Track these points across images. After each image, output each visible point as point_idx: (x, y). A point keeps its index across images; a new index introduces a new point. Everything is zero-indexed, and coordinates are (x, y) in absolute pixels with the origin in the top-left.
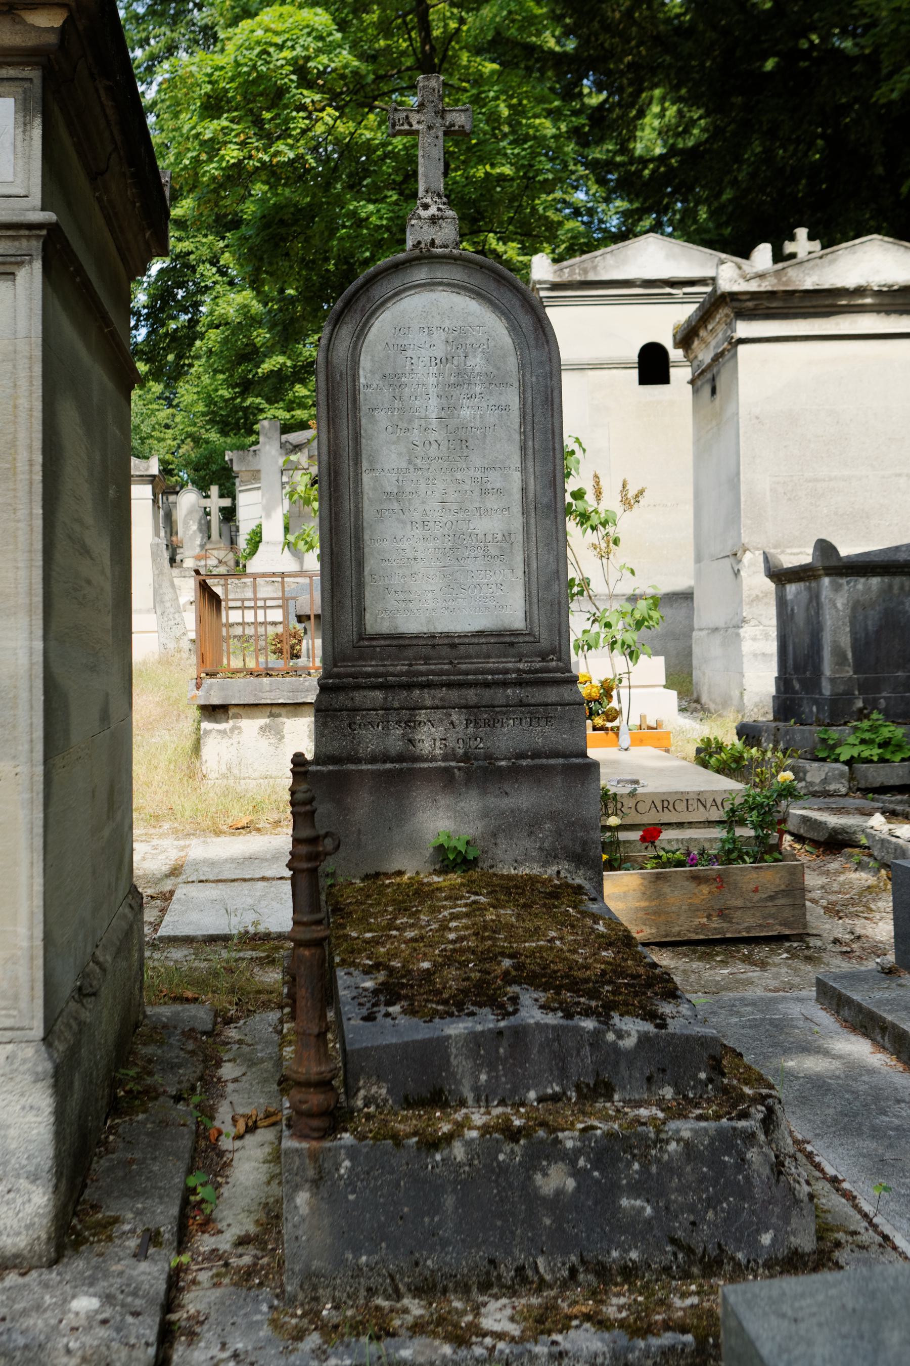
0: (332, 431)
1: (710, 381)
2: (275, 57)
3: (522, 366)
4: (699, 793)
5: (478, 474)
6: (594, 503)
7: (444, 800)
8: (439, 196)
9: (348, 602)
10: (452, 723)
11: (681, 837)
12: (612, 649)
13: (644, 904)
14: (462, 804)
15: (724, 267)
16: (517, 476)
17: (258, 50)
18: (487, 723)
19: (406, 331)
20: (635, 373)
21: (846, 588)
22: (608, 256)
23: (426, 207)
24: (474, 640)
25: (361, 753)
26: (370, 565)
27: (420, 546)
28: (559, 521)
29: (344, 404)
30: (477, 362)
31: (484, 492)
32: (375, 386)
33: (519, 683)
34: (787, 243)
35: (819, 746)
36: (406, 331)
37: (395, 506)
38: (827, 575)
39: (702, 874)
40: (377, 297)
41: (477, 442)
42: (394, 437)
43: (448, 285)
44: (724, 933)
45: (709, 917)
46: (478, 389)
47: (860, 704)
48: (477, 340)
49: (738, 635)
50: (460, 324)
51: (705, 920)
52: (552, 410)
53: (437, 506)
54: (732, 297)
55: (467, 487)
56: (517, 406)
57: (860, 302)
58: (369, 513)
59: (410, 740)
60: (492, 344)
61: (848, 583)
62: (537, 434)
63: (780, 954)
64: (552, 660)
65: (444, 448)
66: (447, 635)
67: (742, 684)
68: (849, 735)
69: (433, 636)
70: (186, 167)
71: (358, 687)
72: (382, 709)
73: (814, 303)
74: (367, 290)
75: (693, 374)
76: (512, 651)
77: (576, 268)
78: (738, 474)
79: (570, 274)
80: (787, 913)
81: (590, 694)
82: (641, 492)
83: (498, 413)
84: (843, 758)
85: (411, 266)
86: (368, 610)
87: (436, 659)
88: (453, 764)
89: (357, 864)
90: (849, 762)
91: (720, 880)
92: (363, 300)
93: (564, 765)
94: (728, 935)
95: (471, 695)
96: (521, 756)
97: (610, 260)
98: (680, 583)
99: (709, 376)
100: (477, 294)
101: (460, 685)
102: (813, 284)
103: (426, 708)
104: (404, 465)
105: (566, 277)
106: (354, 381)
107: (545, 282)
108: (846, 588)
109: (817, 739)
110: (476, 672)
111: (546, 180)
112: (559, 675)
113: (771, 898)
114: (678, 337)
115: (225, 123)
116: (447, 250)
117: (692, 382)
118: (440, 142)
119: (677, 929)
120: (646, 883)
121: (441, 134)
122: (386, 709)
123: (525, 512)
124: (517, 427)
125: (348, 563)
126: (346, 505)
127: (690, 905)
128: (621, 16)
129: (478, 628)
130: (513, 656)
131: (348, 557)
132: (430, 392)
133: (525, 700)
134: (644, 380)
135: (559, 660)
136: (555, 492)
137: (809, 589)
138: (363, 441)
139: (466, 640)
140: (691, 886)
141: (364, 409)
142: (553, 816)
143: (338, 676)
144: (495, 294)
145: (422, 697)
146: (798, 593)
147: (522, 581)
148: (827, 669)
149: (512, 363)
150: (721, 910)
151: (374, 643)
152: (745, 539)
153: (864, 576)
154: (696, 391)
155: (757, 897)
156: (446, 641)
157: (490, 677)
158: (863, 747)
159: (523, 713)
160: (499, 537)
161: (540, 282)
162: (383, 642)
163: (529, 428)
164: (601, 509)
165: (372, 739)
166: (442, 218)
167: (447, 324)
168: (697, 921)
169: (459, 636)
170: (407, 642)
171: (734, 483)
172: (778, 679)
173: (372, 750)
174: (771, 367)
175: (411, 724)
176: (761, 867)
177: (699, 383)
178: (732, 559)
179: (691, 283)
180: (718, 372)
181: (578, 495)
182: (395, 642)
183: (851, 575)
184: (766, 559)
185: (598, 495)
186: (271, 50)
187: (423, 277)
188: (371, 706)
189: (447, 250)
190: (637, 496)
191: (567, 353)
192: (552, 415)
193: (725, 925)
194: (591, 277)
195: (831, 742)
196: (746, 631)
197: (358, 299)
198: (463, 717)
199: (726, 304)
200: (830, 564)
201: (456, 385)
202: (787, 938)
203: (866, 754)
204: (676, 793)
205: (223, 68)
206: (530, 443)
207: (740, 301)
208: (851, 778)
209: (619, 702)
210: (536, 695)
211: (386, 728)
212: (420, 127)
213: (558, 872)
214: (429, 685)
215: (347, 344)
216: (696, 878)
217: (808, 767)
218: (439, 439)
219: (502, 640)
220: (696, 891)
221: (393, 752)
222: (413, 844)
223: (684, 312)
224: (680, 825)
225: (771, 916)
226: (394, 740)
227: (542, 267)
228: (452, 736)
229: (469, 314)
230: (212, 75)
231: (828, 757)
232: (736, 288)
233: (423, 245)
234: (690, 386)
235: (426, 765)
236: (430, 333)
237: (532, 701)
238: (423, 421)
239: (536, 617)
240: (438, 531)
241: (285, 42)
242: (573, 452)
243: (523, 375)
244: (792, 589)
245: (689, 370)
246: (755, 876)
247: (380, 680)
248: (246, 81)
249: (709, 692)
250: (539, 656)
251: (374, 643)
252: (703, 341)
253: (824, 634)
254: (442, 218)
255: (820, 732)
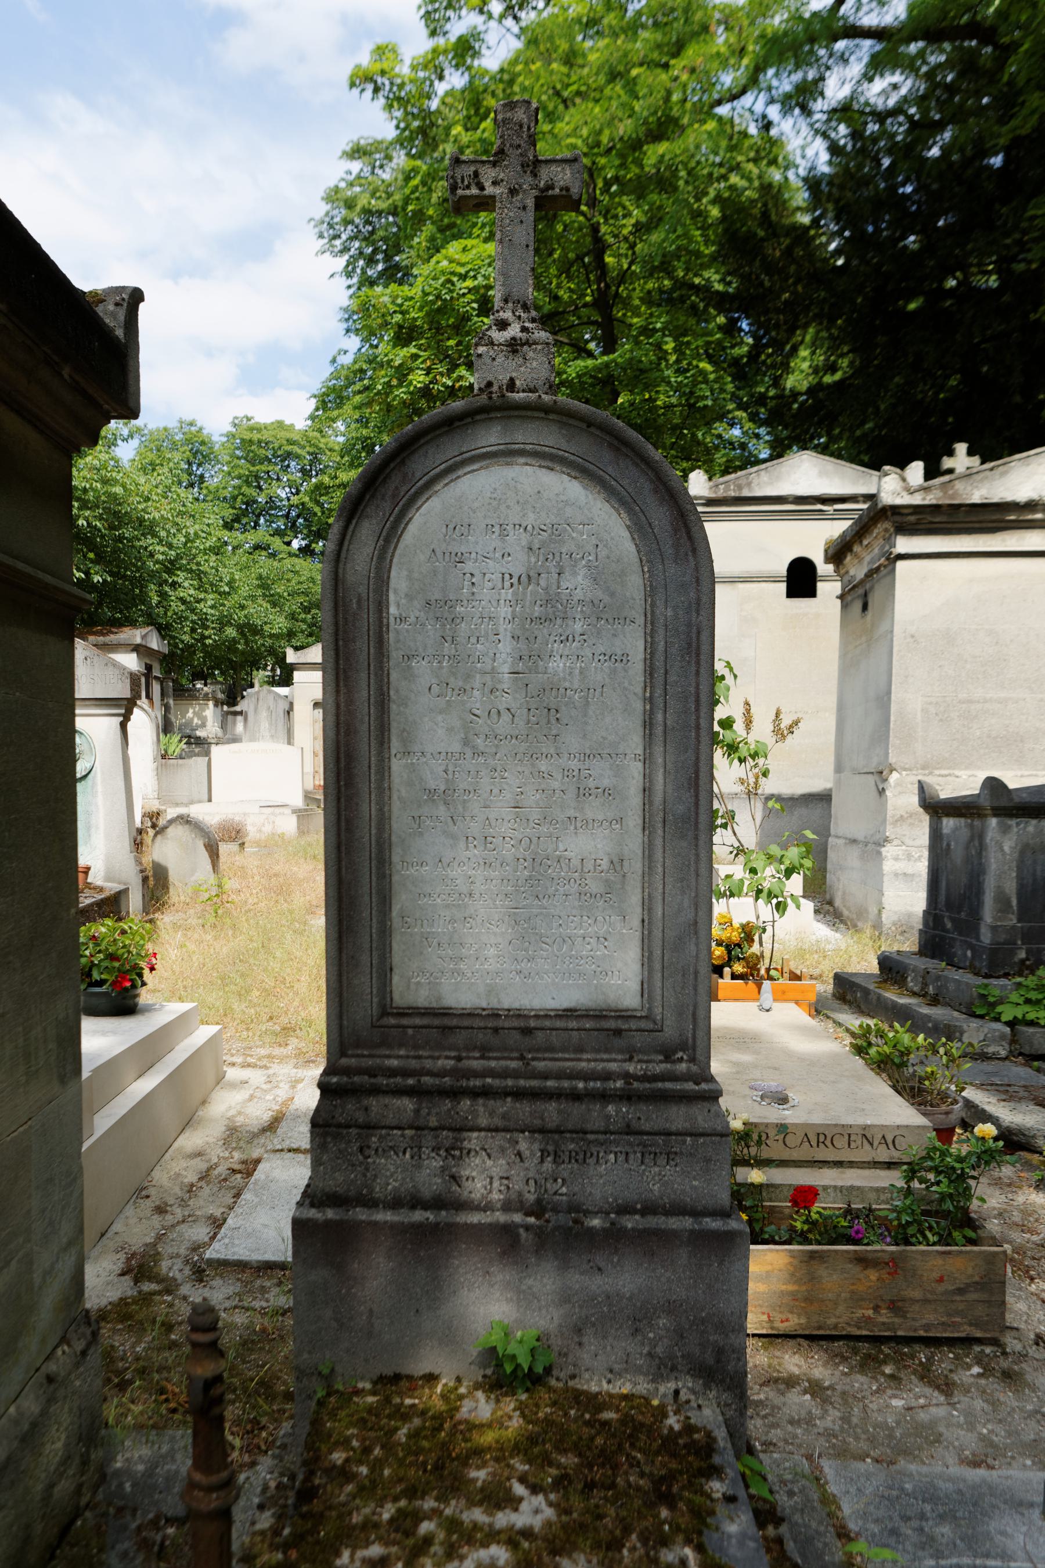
0: (343, 690)
1: (864, 598)
2: (459, 285)
3: (651, 592)
4: (866, 1127)
5: (574, 764)
6: (744, 734)
7: (502, 1275)
8: (525, 307)
9: (365, 958)
10: (519, 1154)
11: (840, 1183)
12: (757, 899)
13: (791, 1288)
14: (530, 1282)
15: (887, 479)
16: (636, 769)
17: (443, 279)
18: (573, 1157)
19: (464, 530)
20: (783, 587)
21: (1015, 830)
22: (763, 473)
23: (503, 325)
24: (559, 1024)
25: (378, 1192)
26: (400, 902)
27: (479, 874)
28: (701, 843)
29: (362, 647)
30: (578, 583)
31: (582, 793)
32: (412, 619)
33: (627, 1097)
34: (945, 458)
35: (977, 1002)
36: (464, 530)
37: (442, 811)
38: (995, 815)
39: (870, 1256)
40: (418, 475)
41: (574, 712)
42: (441, 702)
43: (535, 454)
44: (895, 1330)
45: (876, 1308)
46: (578, 627)
47: (1022, 955)
48: (578, 546)
49: (879, 853)
50: (552, 519)
51: (870, 1312)
52: (698, 663)
53: (507, 813)
54: (895, 510)
55: (556, 785)
56: (641, 656)
57: (1030, 517)
58: (400, 822)
59: (453, 1177)
60: (603, 553)
61: (1018, 824)
62: (671, 703)
63: (969, 1367)
64: (681, 1060)
65: (520, 722)
66: (519, 1014)
67: (880, 903)
68: (1011, 991)
69: (495, 1015)
70: (379, 393)
71: (375, 1091)
72: (411, 1127)
73: (981, 518)
74: (403, 462)
75: (843, 589)
76: (617, 1042)
77: (729, 485)
78: (889, 693)
79: (725, 491)
80: (980, 1311)
81: (730, 938)
82: (796, 723)
83: (607, 668)
84: (1005, 1018)
85: (474, 422)
86: (396, 971)
87: (498, 1050)
88: (518, 1218)
89: (366, 1360)
90: (1012, 1024)
91: (893, 1265)
92: (395, 480)
93: (692, 1232)
94: (900, 1333)
95: (551, 1112)
96: (625, 1210)
97: (764, 477)
98: (817, 785)
99: (860, 591)
100: (582, 471)
101: (535, 1095)
102: (981, 497)
103: (480, 1130)
104: (456, 747)
105: (721, 493)
106: (380, 611)
107: (701, 498)
108: (1015, 830)
109: (975, 994)
110: (560, 1075)
111: (706, 406)
112: (690, 1086)
113: (961, 1291)
114: (830, 552)
115: (414, 351)
116: (533, 396)
117: (841, 597)
118: (530, 215)
119: (832, 1321)
120: (796, 1262)
121: (530, 203)
122: (418, 1128)
123: (646, 826)
124: (639, 690)
125: (367, 898)
126: (365, 807)
127: (852, 1292)
128: (782, 255)
129: (566, 1005)
130: (620, 1051)
131: (366, 889)
132: (501, 630)
133: (634, 1124)
134: (791, 593)
135: (692, 1060)
136: (697, 796)
137: (971, 827)
138: (393, 707)
139: (547, 1023)
140: (855, 1269)
141: (395, 655)
142: (671, 1308)
143: (347, 1071)
144: (610, 470)
145: (475, 1113)
146: (956, 829)
147: (638, 934)
148: (988, 915)
149: (634, 584)
150: (892, 1302)
151: (405, 1021)
152: (892, 759)
153: (1036, 818)
154: (845, 606)
155: (941, 1288)
156: (516, 1023)
157: (581, 1085)
158: (1027, 1008)
159: (631, 1144)
160: (605, 864)
161: (697, 498)
162: (418, 1021)
163: (659, 692)
164: (751, 739)
165: (392, 1173)
166: (527, 343)
167: (531, 519)
168: (859, 1313)
169: (537, 1016)
170: (455, 1022)
171: (884, 700)
172: (926, 913)
173: (395, 1188)
174: (931, 584)
175: (455, 1152)
176: (949, 1253)
177: (849, 598)
178: (876, 777)
179: (843, 499)
180: (872, 588)
181: (727, 724)
182: (437, 1022)
183: (1023, 816)
184: (921, 787)
185: (748, 723)
186: (455, 279)
187: (493, 440)
188: (394, 1123)
189: (533, 396)
190: (791, 726)
191: (721, 566)
192: (698, 673)
193: (896, 1320)
194: (746, 493)
195: (991, 999)
196: (888, 851)
197: (388, 476)
198: (536, 1146)
199: (887, 518)
200: (1000, 802)
201: (542, 620)
202: (979, 1341)
203: (1031, 1016)
204: (836, 1125)
205: (412, 298)
206: (659, 717)
207: (900, 514)
208: (1013, 1041)
209: (761, 944)
210: (651, 1117)
211: (417, 1156)
212: (497, 191)
213: (677, 1392)
214: (485, 1093)
215: (368, 550)
216: (863, 1261)
217: (965, 1027)
218: (513, 706)
219: (603, 1025)
220: (861, 1276)
221: (426, 1193)
222: (449, 1337)
223: (837, 528)
224: (839, 1164)
225: (958, 1313)
226: (428, 1175)
227: (698, 484)
228: (518, 1174)
229: (566, 503)
230: (401, 305)
231: (988, 1014)
232: (898, 501)
233: (495, 388)
234: (839, 601)
235: (475, 1218)
236: (503, 535)
237: (647, 1127)
238: (488, 677)
239: (659, 991)
240: (508, 852)
241: (467, 272)
242: (723, 678)
243: (653, 605)
244: (949, 824)
245: (839, 584)
246: (941, 1262)
247: (411, 1081)
248: (431, 310)
249: (843, 899)
250: (660, 1052)
251: (405, 1021)
252: (856, 556)
253: (987, 877)
254: (527, 343)
255: (979, 987)
